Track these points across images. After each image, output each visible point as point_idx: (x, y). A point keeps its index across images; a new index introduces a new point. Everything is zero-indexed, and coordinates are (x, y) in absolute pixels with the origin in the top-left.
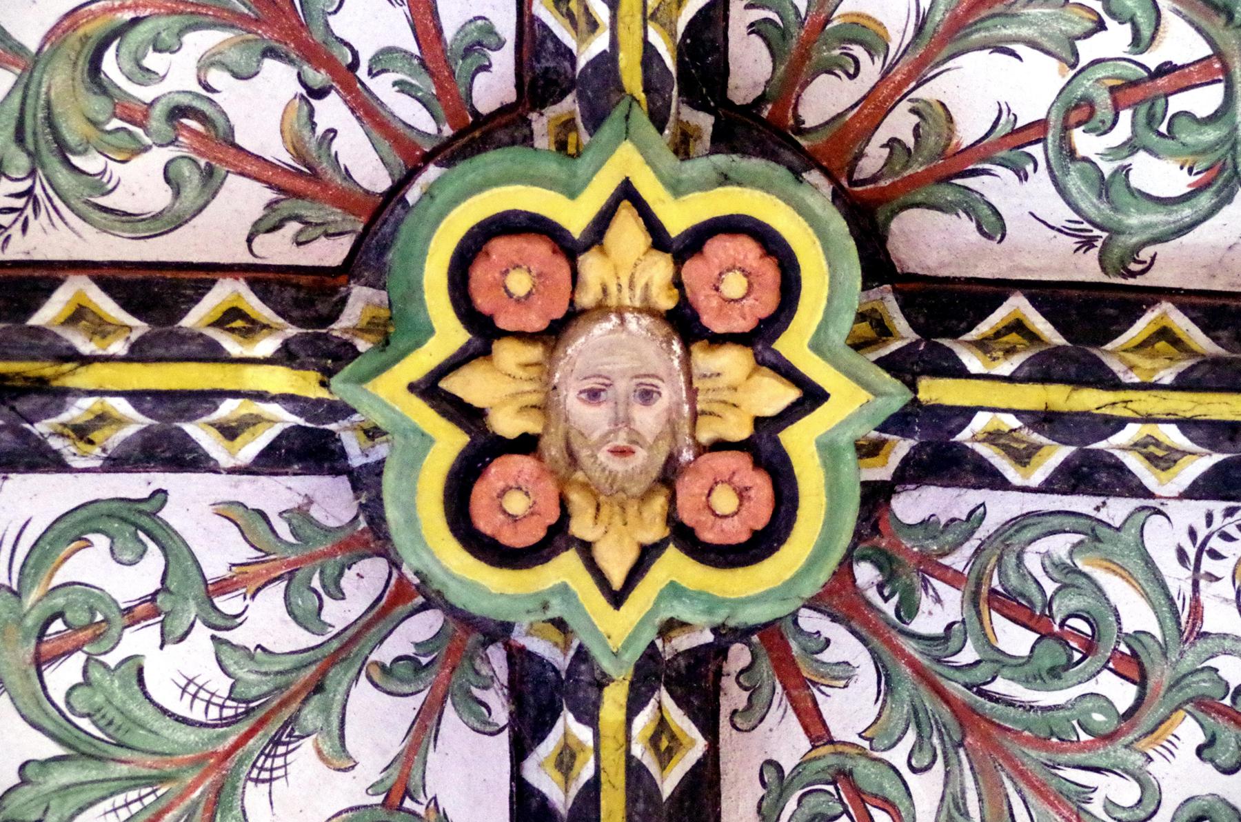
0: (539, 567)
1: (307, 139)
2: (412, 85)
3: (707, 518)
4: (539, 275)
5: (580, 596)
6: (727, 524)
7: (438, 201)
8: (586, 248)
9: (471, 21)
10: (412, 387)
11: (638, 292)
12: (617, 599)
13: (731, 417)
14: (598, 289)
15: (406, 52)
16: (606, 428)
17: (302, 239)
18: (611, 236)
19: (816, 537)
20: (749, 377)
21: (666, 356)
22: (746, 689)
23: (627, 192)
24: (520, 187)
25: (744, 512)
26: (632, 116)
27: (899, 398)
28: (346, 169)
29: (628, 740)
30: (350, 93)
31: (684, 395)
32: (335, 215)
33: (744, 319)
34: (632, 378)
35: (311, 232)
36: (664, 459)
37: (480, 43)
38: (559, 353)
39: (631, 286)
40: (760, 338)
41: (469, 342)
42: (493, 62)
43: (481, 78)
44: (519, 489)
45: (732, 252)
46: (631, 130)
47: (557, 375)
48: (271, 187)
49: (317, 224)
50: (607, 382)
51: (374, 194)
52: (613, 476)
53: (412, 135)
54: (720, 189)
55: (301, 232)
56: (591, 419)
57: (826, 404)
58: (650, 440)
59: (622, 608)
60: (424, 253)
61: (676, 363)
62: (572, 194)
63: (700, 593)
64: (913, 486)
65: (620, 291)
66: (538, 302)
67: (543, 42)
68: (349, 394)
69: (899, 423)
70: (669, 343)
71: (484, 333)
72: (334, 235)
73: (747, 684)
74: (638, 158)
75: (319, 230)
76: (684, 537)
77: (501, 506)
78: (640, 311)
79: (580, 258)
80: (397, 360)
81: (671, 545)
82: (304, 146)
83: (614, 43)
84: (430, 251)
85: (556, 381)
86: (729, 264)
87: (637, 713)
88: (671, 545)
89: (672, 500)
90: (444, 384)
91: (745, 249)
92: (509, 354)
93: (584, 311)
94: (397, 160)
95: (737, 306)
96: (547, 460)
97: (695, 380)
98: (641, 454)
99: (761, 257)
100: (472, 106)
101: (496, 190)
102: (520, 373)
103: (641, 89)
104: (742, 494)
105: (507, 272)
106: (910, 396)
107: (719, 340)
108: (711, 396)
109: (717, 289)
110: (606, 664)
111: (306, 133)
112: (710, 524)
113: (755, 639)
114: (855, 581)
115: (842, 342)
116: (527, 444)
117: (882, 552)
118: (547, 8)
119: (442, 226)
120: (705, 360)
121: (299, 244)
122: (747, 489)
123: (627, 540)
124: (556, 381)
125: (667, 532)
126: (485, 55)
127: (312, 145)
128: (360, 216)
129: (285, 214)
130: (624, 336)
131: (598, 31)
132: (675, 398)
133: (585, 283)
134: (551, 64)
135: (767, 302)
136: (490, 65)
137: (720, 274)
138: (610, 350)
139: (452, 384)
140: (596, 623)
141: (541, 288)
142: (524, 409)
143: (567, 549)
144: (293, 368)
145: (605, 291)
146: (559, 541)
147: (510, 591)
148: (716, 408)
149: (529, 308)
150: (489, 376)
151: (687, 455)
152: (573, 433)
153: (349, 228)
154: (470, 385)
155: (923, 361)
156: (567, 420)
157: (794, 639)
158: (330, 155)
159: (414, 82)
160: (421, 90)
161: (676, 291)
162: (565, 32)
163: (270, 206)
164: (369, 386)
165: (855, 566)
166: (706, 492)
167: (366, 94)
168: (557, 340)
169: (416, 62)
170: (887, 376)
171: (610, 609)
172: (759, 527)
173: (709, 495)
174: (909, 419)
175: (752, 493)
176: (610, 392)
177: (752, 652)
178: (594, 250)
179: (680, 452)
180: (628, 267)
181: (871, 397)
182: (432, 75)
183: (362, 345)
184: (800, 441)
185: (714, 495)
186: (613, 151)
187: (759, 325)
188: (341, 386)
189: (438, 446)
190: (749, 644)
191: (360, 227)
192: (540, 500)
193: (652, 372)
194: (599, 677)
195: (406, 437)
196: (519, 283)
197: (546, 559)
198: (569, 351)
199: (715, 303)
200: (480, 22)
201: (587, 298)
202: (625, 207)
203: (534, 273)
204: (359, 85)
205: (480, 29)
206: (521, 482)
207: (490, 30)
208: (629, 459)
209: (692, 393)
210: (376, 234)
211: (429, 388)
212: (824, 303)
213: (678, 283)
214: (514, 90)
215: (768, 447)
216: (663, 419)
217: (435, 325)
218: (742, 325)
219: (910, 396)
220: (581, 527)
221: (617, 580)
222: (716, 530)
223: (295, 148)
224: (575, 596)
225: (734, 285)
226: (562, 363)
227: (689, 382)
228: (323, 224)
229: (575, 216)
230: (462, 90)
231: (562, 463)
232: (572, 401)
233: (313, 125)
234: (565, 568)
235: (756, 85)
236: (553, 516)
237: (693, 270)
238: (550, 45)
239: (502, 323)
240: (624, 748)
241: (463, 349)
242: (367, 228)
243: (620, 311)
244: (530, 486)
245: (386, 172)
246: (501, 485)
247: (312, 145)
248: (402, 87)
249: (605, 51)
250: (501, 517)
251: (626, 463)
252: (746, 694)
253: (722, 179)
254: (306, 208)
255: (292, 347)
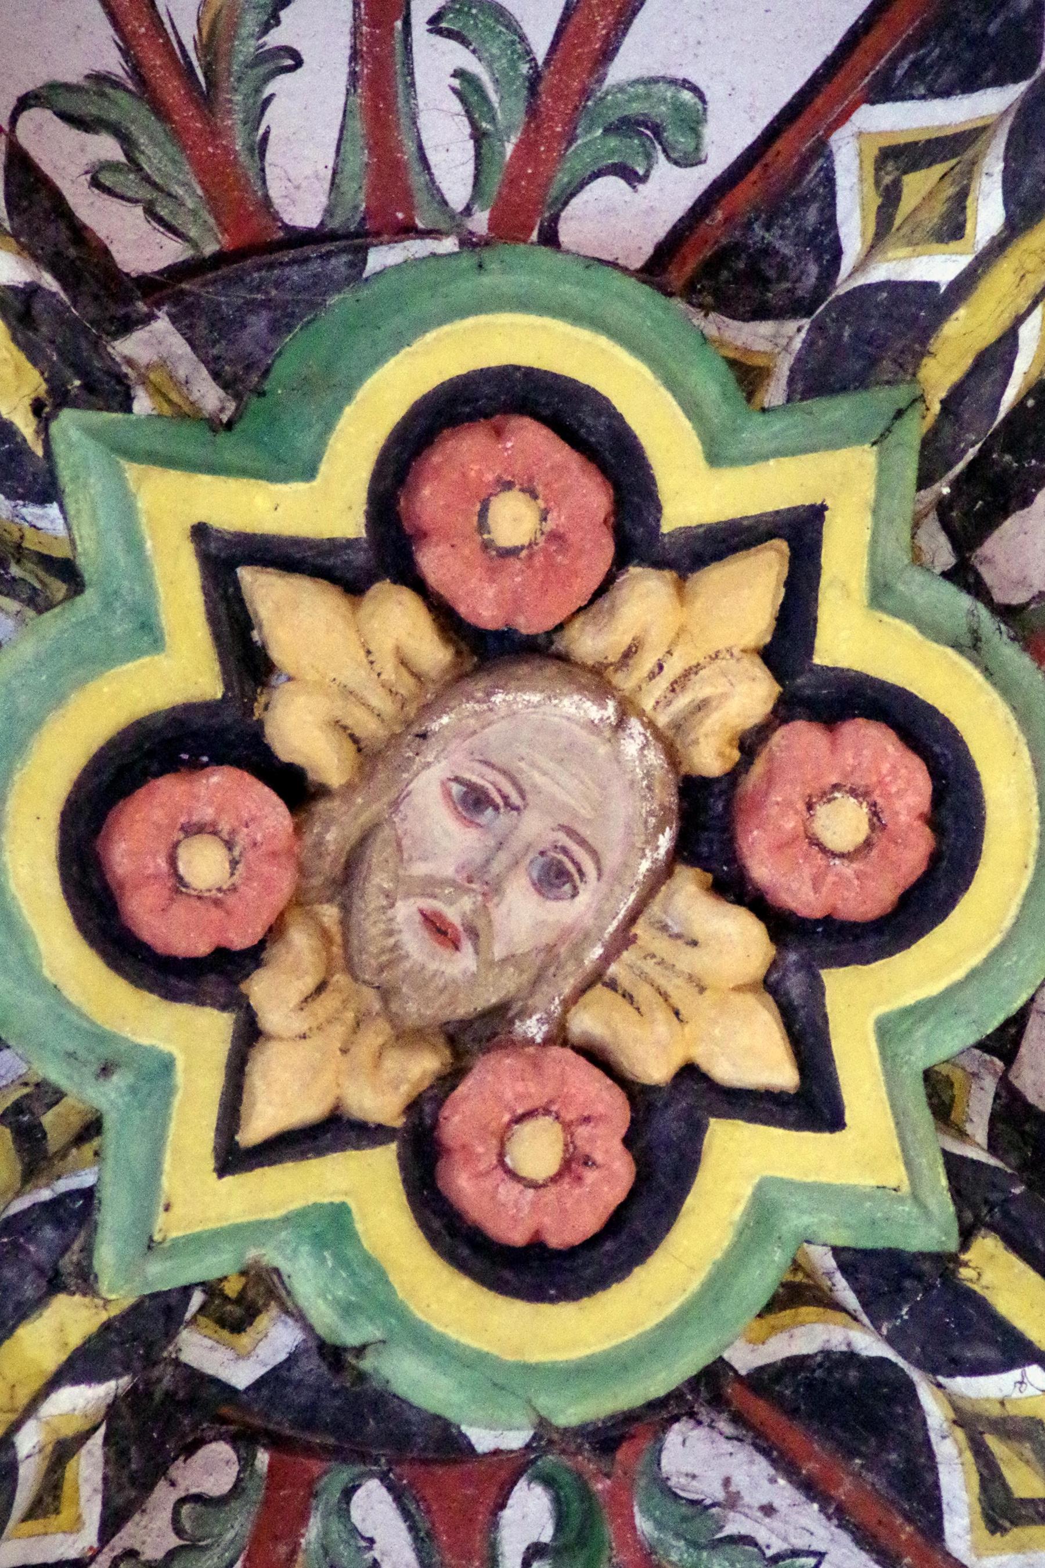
0: (154, 998)
1: (244, 32)
2: (485, 99)
3: (485, 1152)
4: (555, 537)
5: (177, 1101)
6: (508, 1191)
7: (486, 280)
8: (658, 564)
9: (673, 82)
10: (200, 532)
11: (682, 701)
12: (233, 1158)
13: (662, 1025)
14: (627, 640)
15: (523, 39)
16: (448, 871)
17: (107, 179)
18: (715, 578)
19: (631, 1335)
20: (738, 989)
21: (639, 841)
22: (179, 1531)
23: (800, 532)
24: (644, 370)
25: (550, 1194)
26: (906, 419)
27: (934, 1231)
28: (267, 133)
29: (31, 1409)
30: (374, 24)
31: (611, 929)
32: (188, 190)
33: (816, 888)
34: (563, 827)
35: (128, 183)
36: (494, 1000)
37: (657, 131)
38: (478, 686)
39: (675, 687)
40: (809, 943)
41: (350, 544)
42: (655, 173)
43: (610, 187)
44: (229, 845)
45: (885, 767)
46: (892, 439)
47: (445, 720)
48: (125, 53)
49: (147, 179)
50: (515, 798)
51: (276, 217)
52: (395, 954)
53: (416, 180)
54: (950, 652)
55: (112, 166)
56: (437, 835)
57: (826, 1136)
58: (499, 951)
59: (228, 1179)
60: (400, 341)
61: (645, 865)
62: (716, 456)
63: (369, 1262)
64: (729, 1429)
65: (652, 676)
66: (515, 575)
67: (803, 201)
68: (75, 457)
69: (883, 1276)
70: (659, 829)
71: (385, 554)
72: (160, 220)
73: (187, 1526)
74: (868, 490)
75: (145, 193)
76: (422, 1147)
77: (176, 845)
78: (658, 734)
79: (634, 570)
80: (212, 469)
81: (394, 1146)
82: (231, 38)
83: (965, 285)
84: (418, 345)
85: (435, 726)
86: (859, 780)
87: (76, 1381)
88: (394, 1146)
89: (450, 1079)
90: (246, 574)
91: (910, 787)
92: (398, 620)
93: (563, 658)
94: (357, 196)
95: (819, 859)
96: (309, 840)
97: (641, 920)
98: (464, 962)
99: (921, 816)
100: (555, 219)
101: (603, 341)
102: (390, 671)
103: (943, 395)
104: (574, 1164)
105: (508, 486)
106: (952, 1245)
107: (733, 886)
108: (649, 966)
109: (810, 807)
110: (107, 1256)
111: (251, 22)
112: (482, 1167)
113: (263, 1459)
114: (503, 1506)
115: (922, 1065)
116: (295, 788)
117: (586, 1495)
118: (860, 153)
119: (470, 321)
120: (689, 898)
121: (96, 183)
122: (587, 1161)
123: (327, 1078)
124: (435, 726)
125: (399, 1123)
126: (649, 157)
127: (246, 49)
128: (225, 230)
129: (113, 116)
130: (603, 750)
131: (953, 245)
132: (589, 921)
133: (612, 611)
134: (787, 249)
135: (866, 895)
136: (644, 179)
137: (836, 787)
138: (568, 753)
139: (265, 591)
140: (167, 1166)
141: (539, 560)
142: (339, 726)
143: (223, 1008)
144: (14, 339)
145: (629, 654)
146: (211, 982)
147: (73, 993)
148: (644, 993)
149: (492, 573)
150: (340, 624)
151: (533, 1028)
152: (386, 832)
153: (193, 233)
154: (292, 615)
155: (1006, 1214)
156: (395, 805)
157: (325, 1517)
158: (258, 91)
159: (494, 98)
160: (493, 120)
161: (736, 755)
162: (857, 215)
163: (100, 79)
164: (132, 471)
165: (522, 1483)
166: (520, 1111)
167: (399, 47)
168: (478, 669)
169: (524, 68)
170: (944, 1182)
171: (210, 1163)
172: (555, 1241)
173: (519, 1119)
174: (908, 1284)
175: (591, 1176)
176: (504, 820)
177: (239, 1480)
178: (669, 575)
179: (524, 1013)
180: (336, 662)
181: (906, 1188)
182: (532, 112)
183: (143, 404)
184: (738, 1158)
185: (526, 1129)
186: (832, 446)
187: (817, 922)
188: (75, 434)
189: (160, 661)
190: (246, 1463)
191: (210, 249)
192: (250, 892)
193: (598, 845)
194: (68, 1262)
195: (107, 606)
196: (514, 520)
197: (172, 995)
198: (498, 698)
199: (790, 824)
200: (687, 96)
201: (588, 642)
202: (778, 551)
203: (549, 526)
204: (399, 24)
205: (678, 107)
206: (242, 840)
207: (693, 122)
208: (446, 953)
209: (624, 939)
210: (271, 266)
211: (224, 558)
212: (959, 974)
213: (750, 744)
214: (648, 250)
215: (668, 1124)
216: (547, 937)
217: (323, 468)
218: (801, 894)
219: (952, 1245)
220: (273, 994)
221: (260, 1124)
222: (488, 1184)
223: (212, 32)
224: (169, 1092)
225: (844, 823)
226: (470, 706)
227: (632, 918)
228: (155, 185)
229: (691, 494)
230: (563, 178)
231: (328, 866)
232: (428, 786)
233: (272, 21)
234: (193, 1036)
235: (1022, 582)
236: (240, 940)
237: (801, 738)
238: (812, 216)
239: (433, 562)
240: (13, 1417)
241: (335, 546)
242: (220, 259)
243: (626, 708)
244: (251, 855)
245: (323, 200)
246: (207, 813)
247: (246, 49)
248: (467, 89)
249: (934, 286)
250: (162, 863)
251: (433, 956)
252: (173, 1541)
253: (967, 640)
254: (151, 138)
255: (38, 306)
